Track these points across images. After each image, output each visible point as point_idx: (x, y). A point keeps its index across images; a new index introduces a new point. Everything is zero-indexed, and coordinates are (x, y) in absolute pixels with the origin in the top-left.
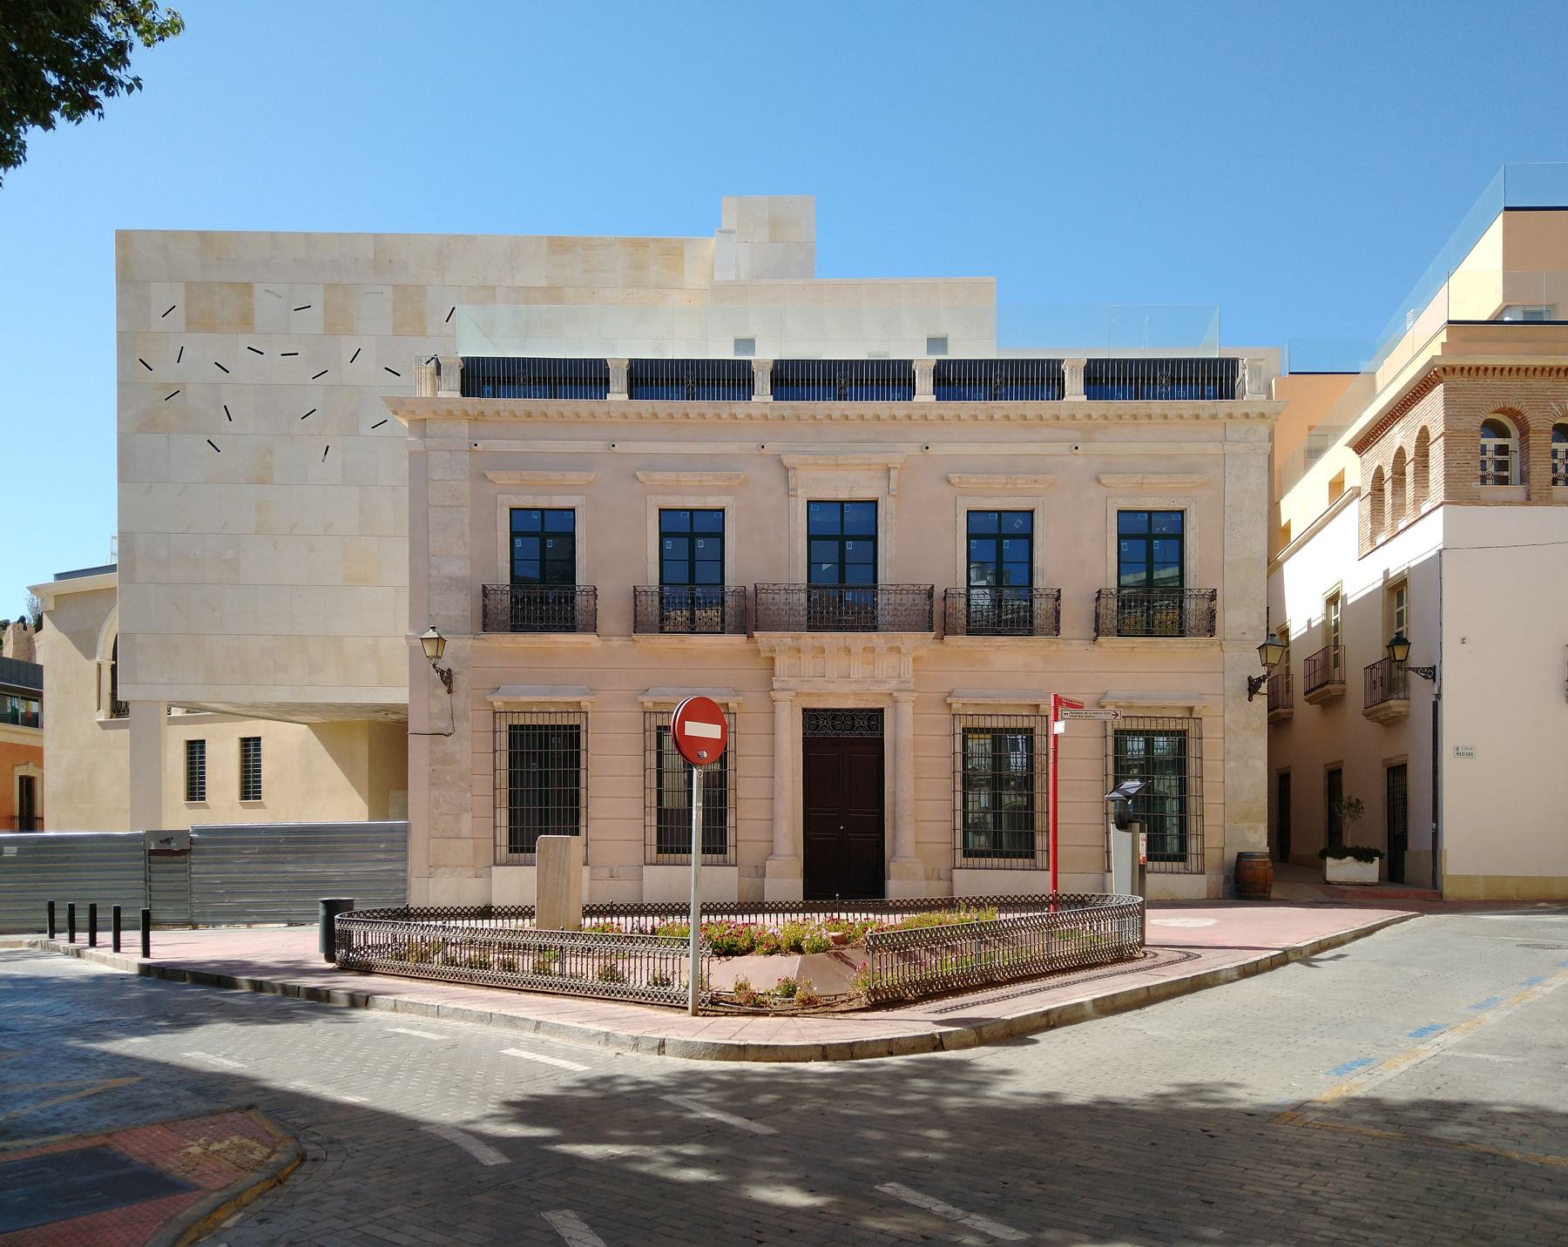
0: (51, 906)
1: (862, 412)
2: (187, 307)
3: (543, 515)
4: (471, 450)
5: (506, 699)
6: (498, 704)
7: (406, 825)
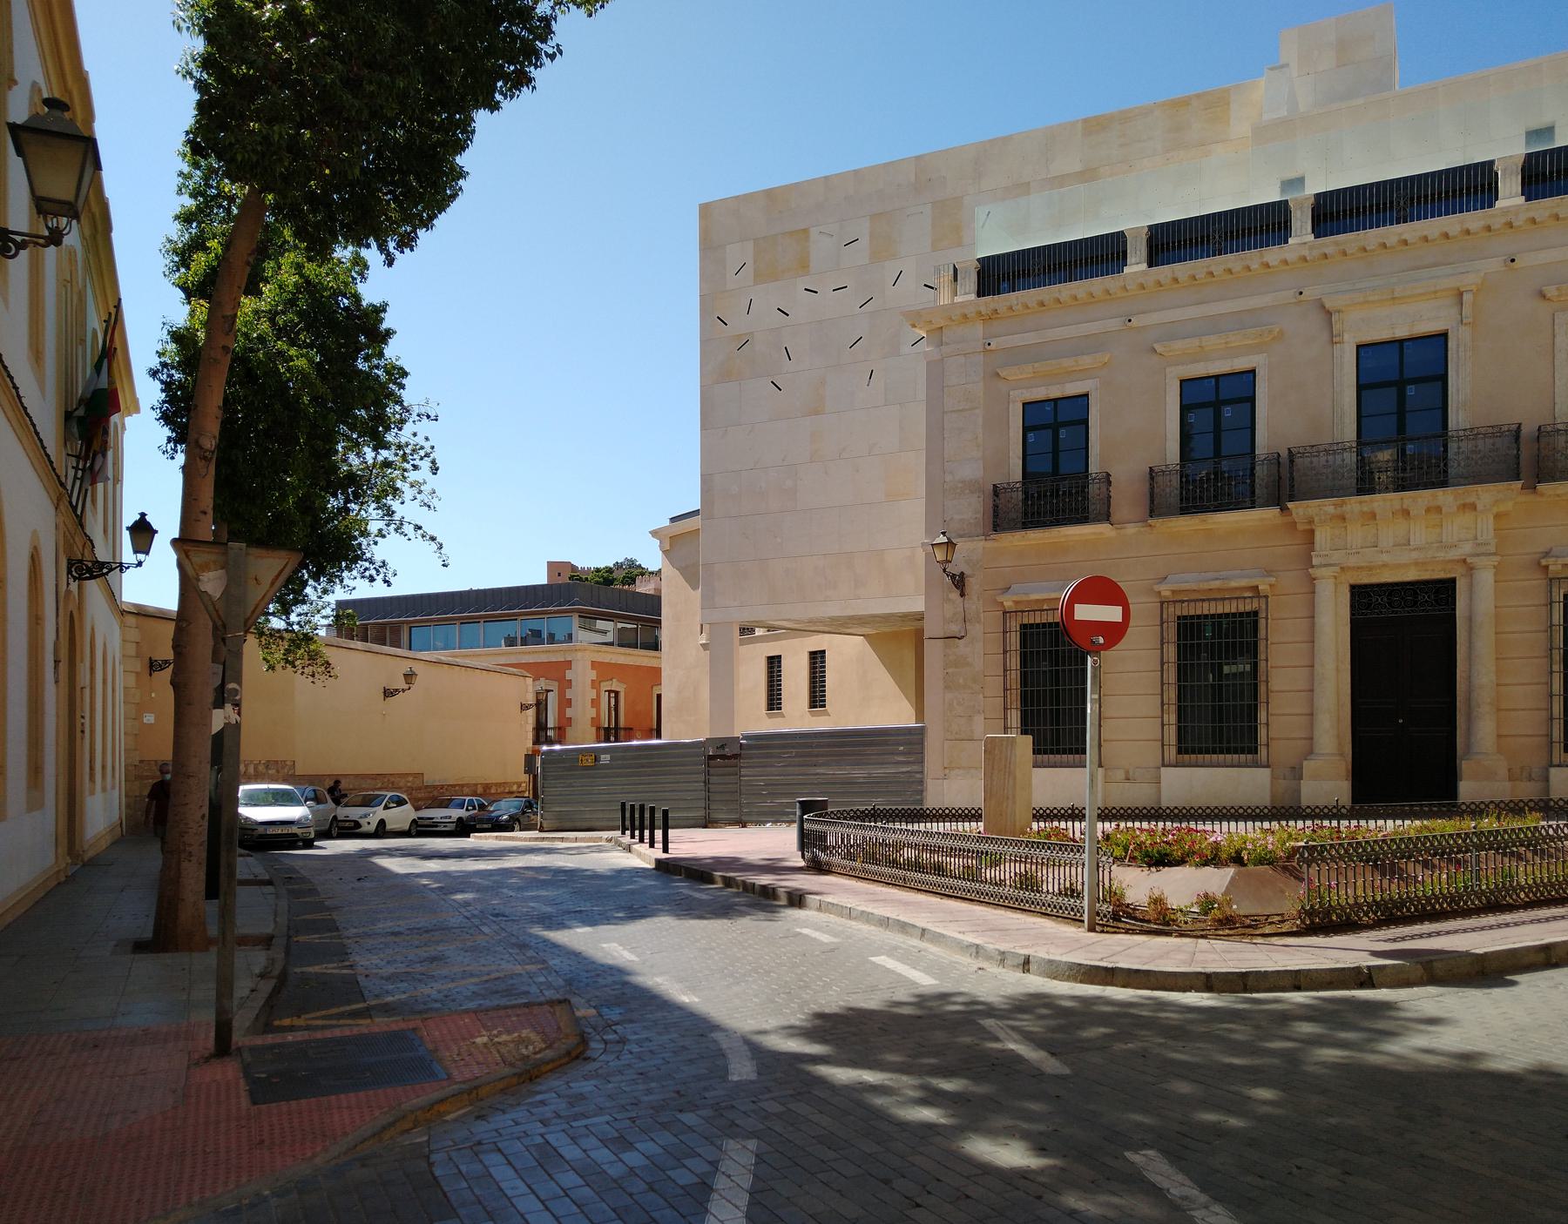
0: (623, 805)
1: (1425, 233)
2: (755, 262)
3: (1056, 406)
4: (985, 351)
5: (1015, 598)
6: (1008, 604)
7: (923, 728)
